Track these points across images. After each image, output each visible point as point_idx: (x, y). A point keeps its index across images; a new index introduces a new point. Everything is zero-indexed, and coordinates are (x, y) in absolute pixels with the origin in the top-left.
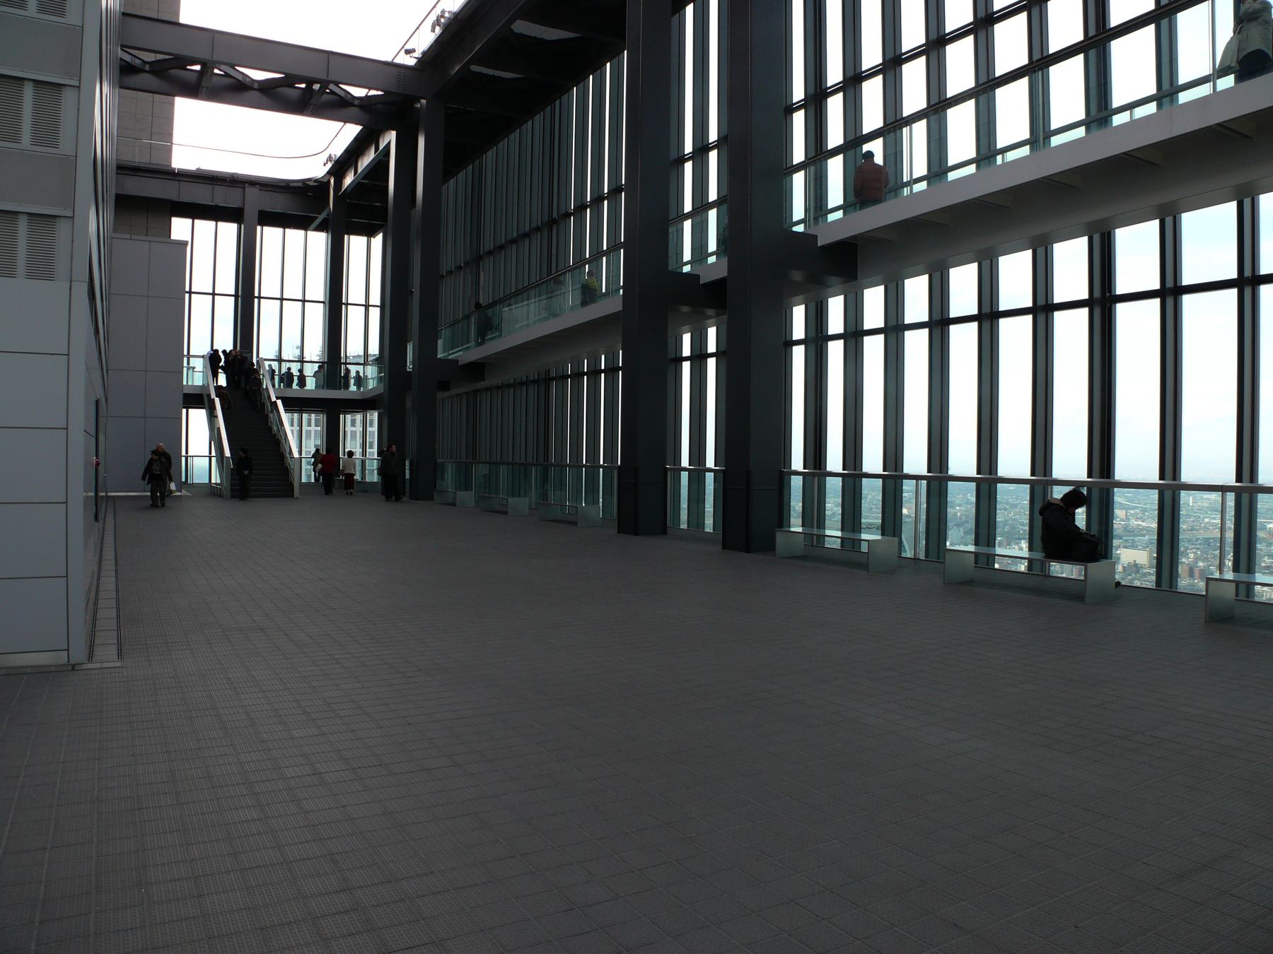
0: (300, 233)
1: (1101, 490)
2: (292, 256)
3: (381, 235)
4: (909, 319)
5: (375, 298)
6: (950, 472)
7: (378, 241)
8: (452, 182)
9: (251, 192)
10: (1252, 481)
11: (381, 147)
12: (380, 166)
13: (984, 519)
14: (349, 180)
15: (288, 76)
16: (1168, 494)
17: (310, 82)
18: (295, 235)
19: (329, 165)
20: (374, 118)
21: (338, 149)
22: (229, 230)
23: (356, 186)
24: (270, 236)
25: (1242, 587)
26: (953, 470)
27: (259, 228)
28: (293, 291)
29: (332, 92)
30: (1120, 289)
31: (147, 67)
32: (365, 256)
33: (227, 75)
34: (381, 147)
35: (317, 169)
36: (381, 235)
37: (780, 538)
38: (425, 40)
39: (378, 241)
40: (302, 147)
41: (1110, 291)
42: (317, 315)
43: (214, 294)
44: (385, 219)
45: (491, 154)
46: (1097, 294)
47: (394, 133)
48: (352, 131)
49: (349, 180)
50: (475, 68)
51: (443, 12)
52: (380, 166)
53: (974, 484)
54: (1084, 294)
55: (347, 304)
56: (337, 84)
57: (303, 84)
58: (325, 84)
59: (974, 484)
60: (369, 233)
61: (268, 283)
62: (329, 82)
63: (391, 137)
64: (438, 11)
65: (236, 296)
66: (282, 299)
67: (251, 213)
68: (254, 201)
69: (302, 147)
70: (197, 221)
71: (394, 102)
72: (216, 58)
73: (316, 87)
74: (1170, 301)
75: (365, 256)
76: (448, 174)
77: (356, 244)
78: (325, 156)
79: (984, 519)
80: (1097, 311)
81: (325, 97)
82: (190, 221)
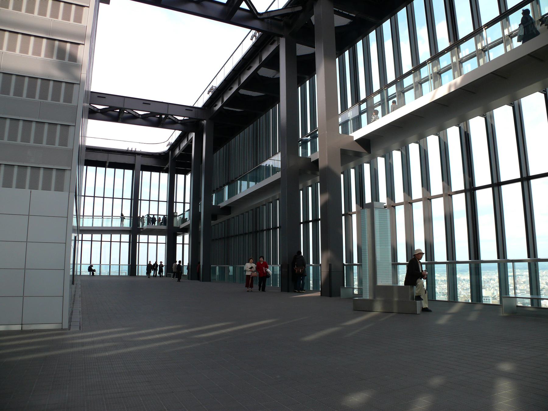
0: (94, 168)
1: (476, 264)
2: (155, 184)
3: (190, 174)
4: (421, 203)
5: (188, 200)
6: (398, 262)
7: (189, 177)
8: (218, 152)
9: (138, 157)
10: (535, 257)
11: (189, 139)
12: (189, 147)
13: (503, 277)
14: (177, 152)
15: (110, 107)
16: (533, 264)
17: (161, 115)
18: (155, 175)
19: (169, 147)
20: (186, 127)
21: (173, 140)
22: (129, 173)
23: (180, 155)
24: (146, 175)
25: (535, 301)
26: (458, 259)
27: (85, 167)
28: (154, 197)
29: (170, 118)
30: (477, 185)
31: (140, 116)
32: (184, 182)
33: (129, 113)
34: (189, 139)
35: (163, 148)
36: (190, 174)
37: (342, 291)
38: (206, 97)
39: (189, 177)
40: (157, 140)
41: (473, 186)
42: (127, 204)
43: (94, 197)
44: (189, 165)
45: (233, 140)
46: (468, 187)
47: (194, 134)
48: (178, 133)
49: (177, 152)
50: (225, 108)
51: (212, 87)
52: (189, 147)
53: (496, 264)
54: (462, 188)
55: (141, 200)
56: (172, 115)
57: (156, 115)
58: (167, 116)
59: (496, 264)
60: (185, 174)
61: (144, 194)
62: (125, 109)
63: (193, 135)
64: (210, 86)
65: (131, 199)
66: (150, 200)
67: (138, 166)
68: (139, 161)
69: (157, 140)
70: (152, 173)
71: (191, 121)
72: (125, 107)
73: (163, 116)
74: (496, 189)
75: (184, 182)
76: (215, 150)
77: (180, 178)
78: (167, 143)
79: (503, 277)
80: (468, 194)
81: (167, 120)
82: (150, 173)
